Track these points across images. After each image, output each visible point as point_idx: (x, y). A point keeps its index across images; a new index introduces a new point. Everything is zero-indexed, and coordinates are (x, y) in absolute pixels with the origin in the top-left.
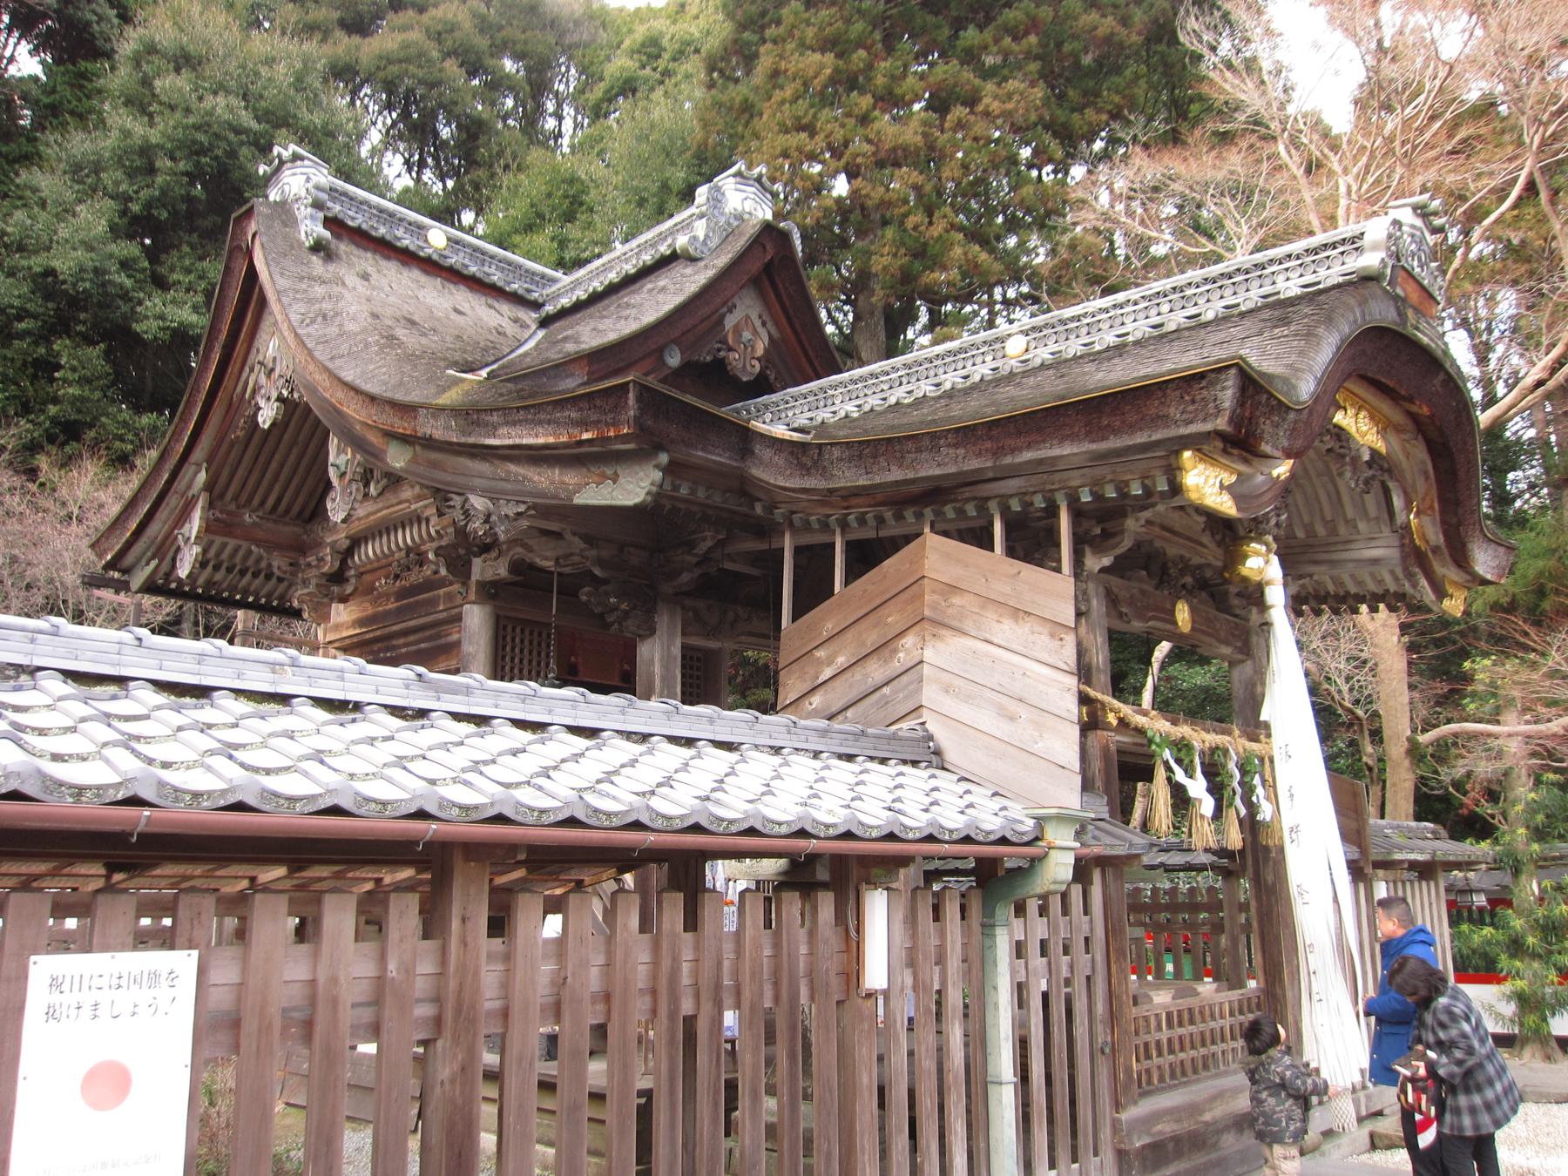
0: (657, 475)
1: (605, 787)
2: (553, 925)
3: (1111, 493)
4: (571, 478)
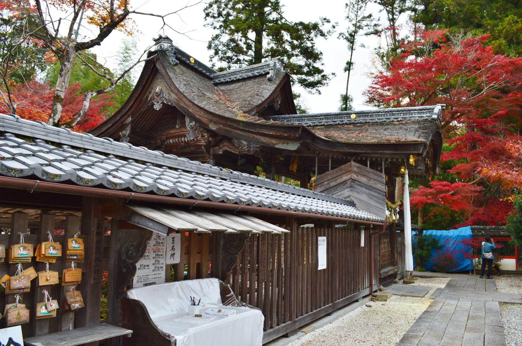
0: (299, 145)
1: (115, 173)
2: (400, 239)
3: (400, 160)
4: (274, 141)
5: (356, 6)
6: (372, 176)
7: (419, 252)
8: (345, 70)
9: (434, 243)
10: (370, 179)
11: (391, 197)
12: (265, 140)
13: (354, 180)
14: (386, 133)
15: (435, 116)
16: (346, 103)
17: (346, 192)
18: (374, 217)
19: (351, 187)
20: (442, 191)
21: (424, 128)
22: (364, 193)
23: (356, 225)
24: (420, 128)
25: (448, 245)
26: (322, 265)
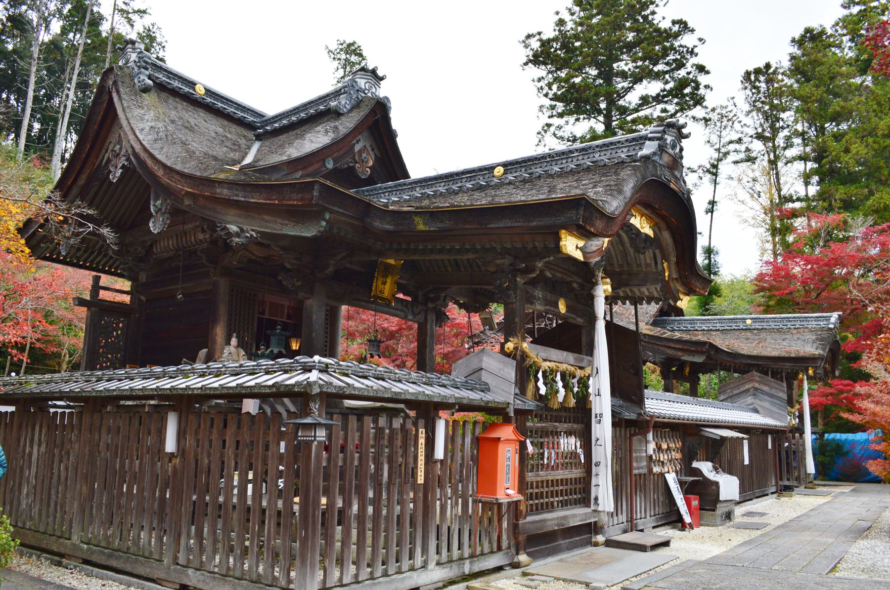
4: (680, 354)
5: (718, 124)
6: (773, 385)
7: (821, 458)
8: (707, 212)
9: (838, 449)
10: (772, 387)
11: (790, 402)
12: (670, 352)
13: (756, 389)
14: (785, 343)
15: (832, 326)
16: (709, 258)
17: (750, 400)
18: (778, 423)
19: (754, 395)
20: (842, 392)
21: (821, 340)
22: (766, 400)
23: (765, 431)
24: (817, 339)
25: (854, 451)
26: (747, 462)
